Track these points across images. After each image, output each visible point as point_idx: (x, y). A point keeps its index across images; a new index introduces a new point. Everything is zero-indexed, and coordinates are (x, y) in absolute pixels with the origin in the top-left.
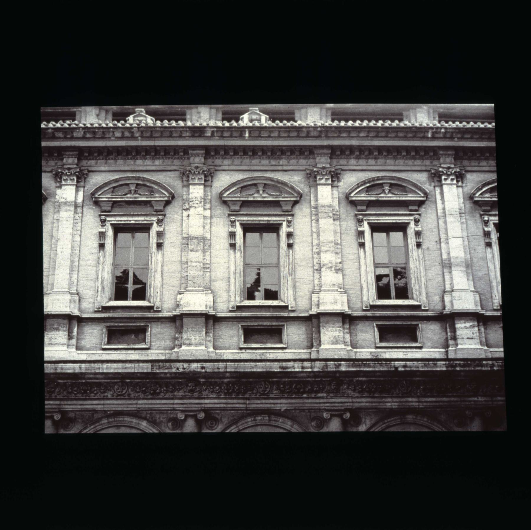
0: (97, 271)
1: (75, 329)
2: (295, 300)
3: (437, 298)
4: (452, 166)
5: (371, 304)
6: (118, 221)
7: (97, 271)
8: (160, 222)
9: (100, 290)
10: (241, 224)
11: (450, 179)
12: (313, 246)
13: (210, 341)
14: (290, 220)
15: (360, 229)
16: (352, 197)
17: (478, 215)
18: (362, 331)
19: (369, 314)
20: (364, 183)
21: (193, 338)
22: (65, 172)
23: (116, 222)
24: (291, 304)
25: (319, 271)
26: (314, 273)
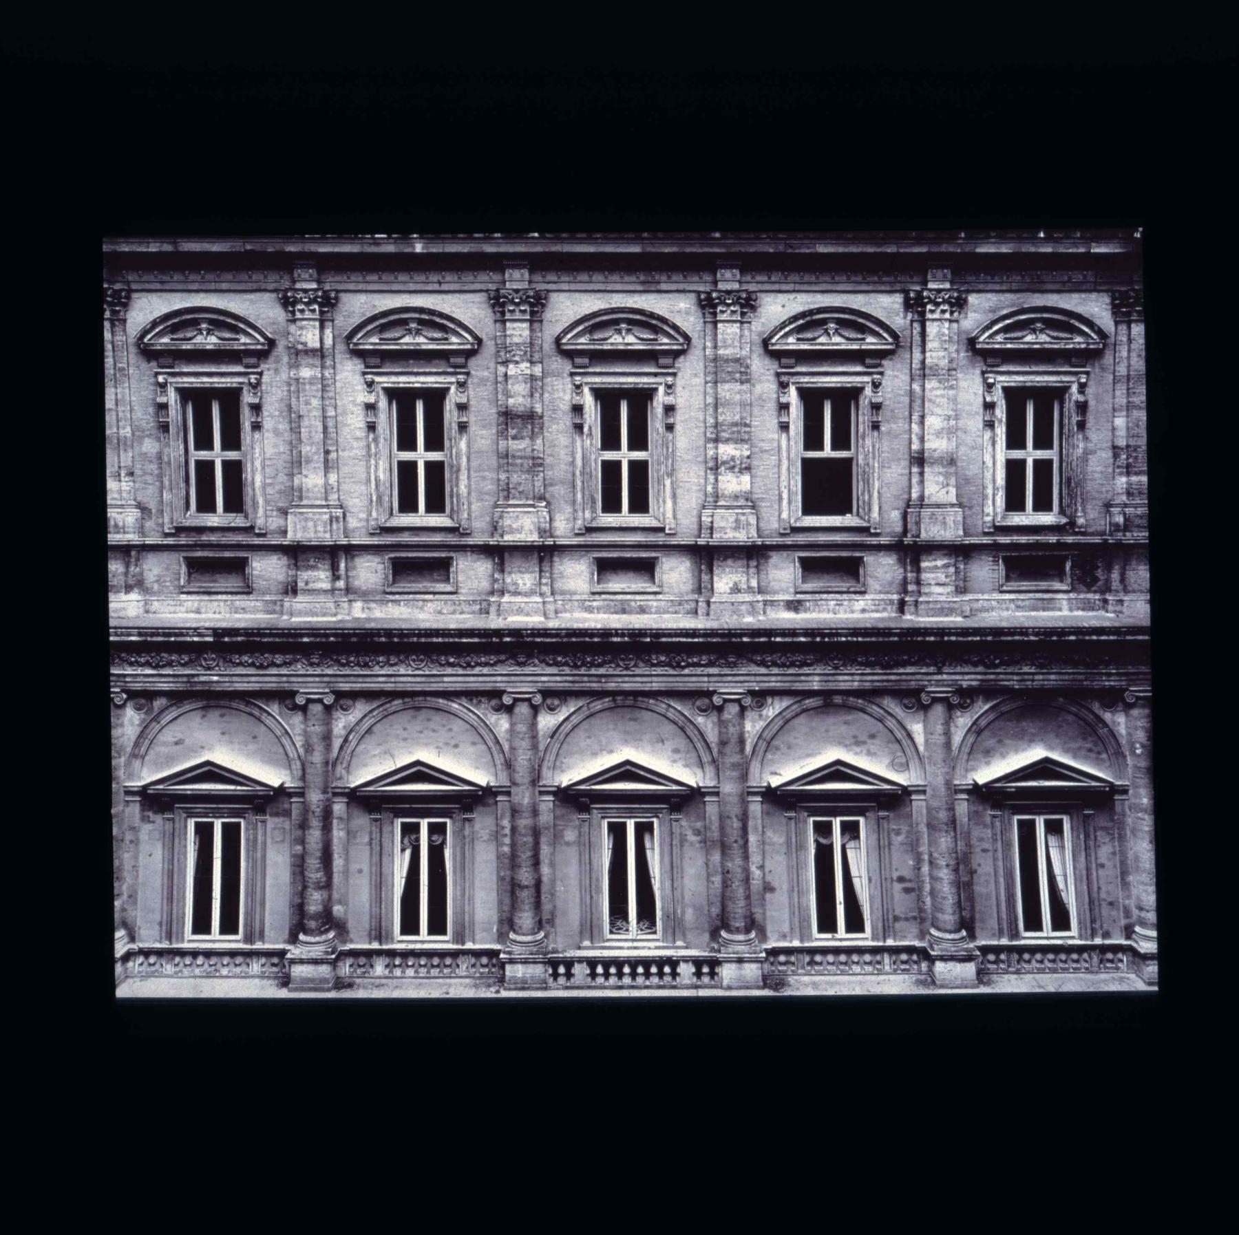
0: (368, 468)
1: (342, 565)
2: (675, 517)
3: (895, 515)
4: (947, 286)
5: (794, 525)
6: (394, 383)
7: (368, 468)
8: (462, 385)
9: (374, 498)
10: (592, 389)
11: (939, 311)
12: (706, 427)
13: (546, 584)
14: (670, 383)
15: (783, 400)
16: (773, 344)
17: (978, 372)
18: (776, 567)
19: (789, 540)
20: (795, 318)
21: (520, 582)
22: (298, 296)
23: (390, 385)
24: (670, 524)
25: (715, 469)
26: (706, 472)
